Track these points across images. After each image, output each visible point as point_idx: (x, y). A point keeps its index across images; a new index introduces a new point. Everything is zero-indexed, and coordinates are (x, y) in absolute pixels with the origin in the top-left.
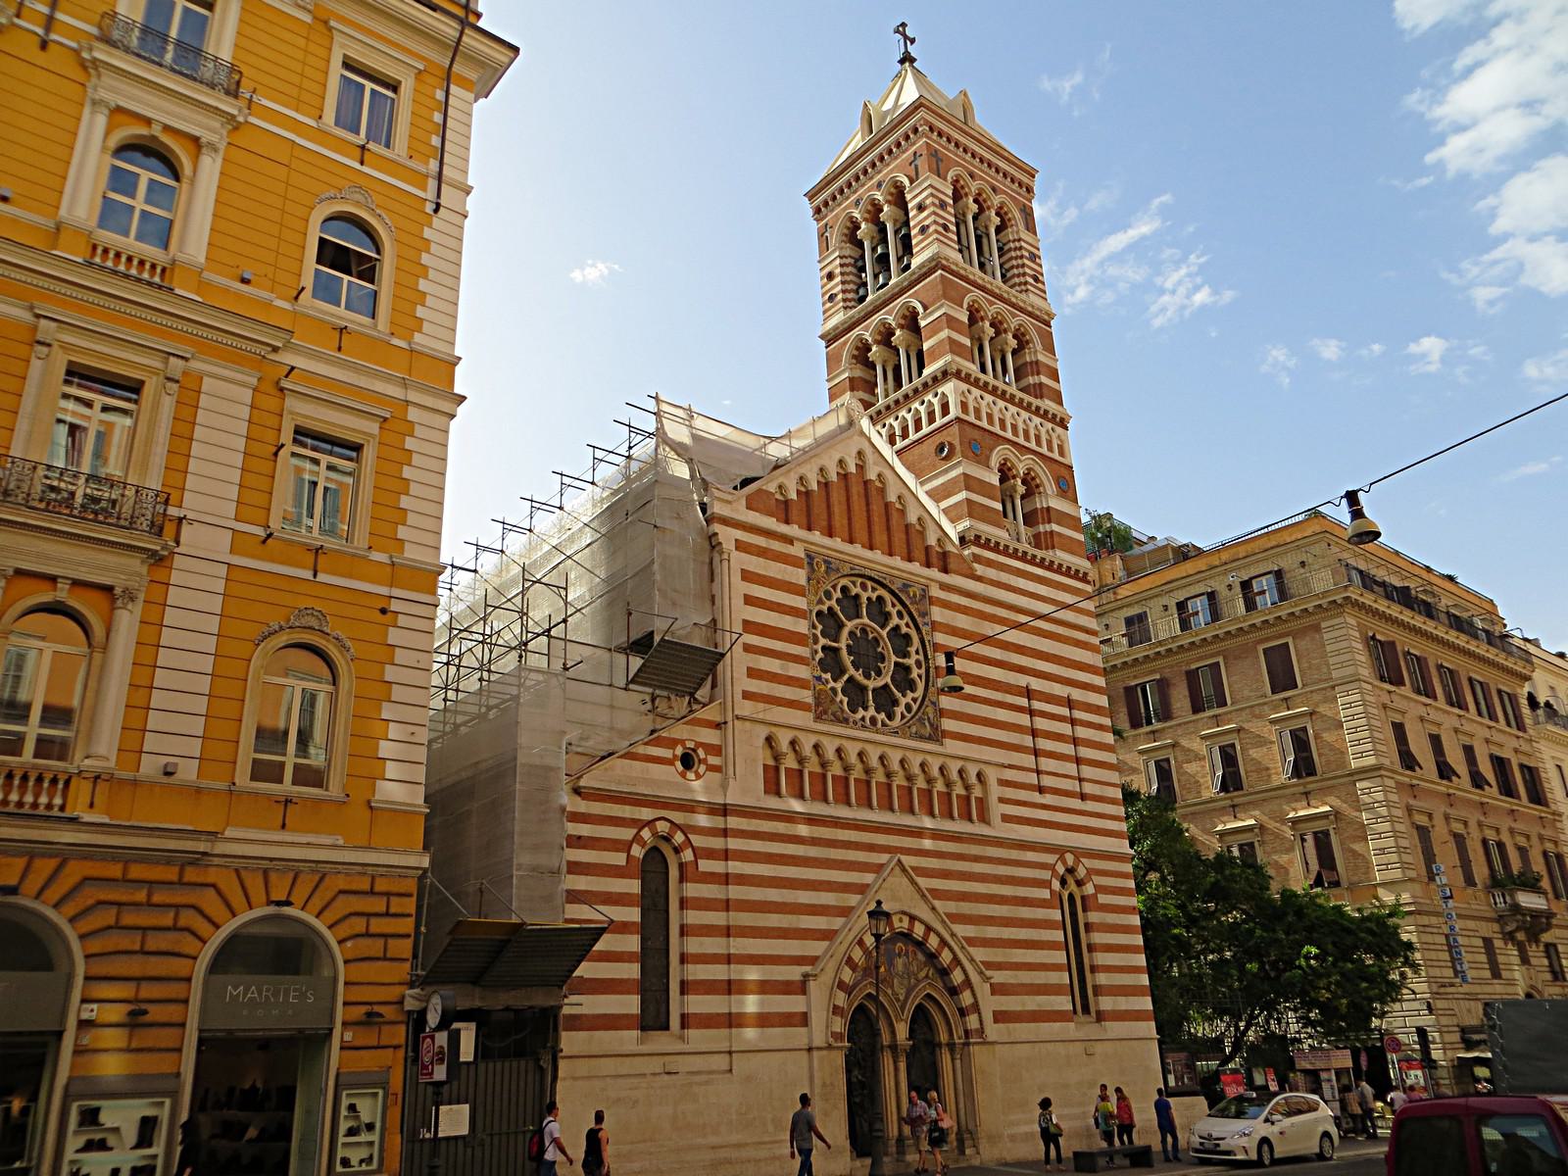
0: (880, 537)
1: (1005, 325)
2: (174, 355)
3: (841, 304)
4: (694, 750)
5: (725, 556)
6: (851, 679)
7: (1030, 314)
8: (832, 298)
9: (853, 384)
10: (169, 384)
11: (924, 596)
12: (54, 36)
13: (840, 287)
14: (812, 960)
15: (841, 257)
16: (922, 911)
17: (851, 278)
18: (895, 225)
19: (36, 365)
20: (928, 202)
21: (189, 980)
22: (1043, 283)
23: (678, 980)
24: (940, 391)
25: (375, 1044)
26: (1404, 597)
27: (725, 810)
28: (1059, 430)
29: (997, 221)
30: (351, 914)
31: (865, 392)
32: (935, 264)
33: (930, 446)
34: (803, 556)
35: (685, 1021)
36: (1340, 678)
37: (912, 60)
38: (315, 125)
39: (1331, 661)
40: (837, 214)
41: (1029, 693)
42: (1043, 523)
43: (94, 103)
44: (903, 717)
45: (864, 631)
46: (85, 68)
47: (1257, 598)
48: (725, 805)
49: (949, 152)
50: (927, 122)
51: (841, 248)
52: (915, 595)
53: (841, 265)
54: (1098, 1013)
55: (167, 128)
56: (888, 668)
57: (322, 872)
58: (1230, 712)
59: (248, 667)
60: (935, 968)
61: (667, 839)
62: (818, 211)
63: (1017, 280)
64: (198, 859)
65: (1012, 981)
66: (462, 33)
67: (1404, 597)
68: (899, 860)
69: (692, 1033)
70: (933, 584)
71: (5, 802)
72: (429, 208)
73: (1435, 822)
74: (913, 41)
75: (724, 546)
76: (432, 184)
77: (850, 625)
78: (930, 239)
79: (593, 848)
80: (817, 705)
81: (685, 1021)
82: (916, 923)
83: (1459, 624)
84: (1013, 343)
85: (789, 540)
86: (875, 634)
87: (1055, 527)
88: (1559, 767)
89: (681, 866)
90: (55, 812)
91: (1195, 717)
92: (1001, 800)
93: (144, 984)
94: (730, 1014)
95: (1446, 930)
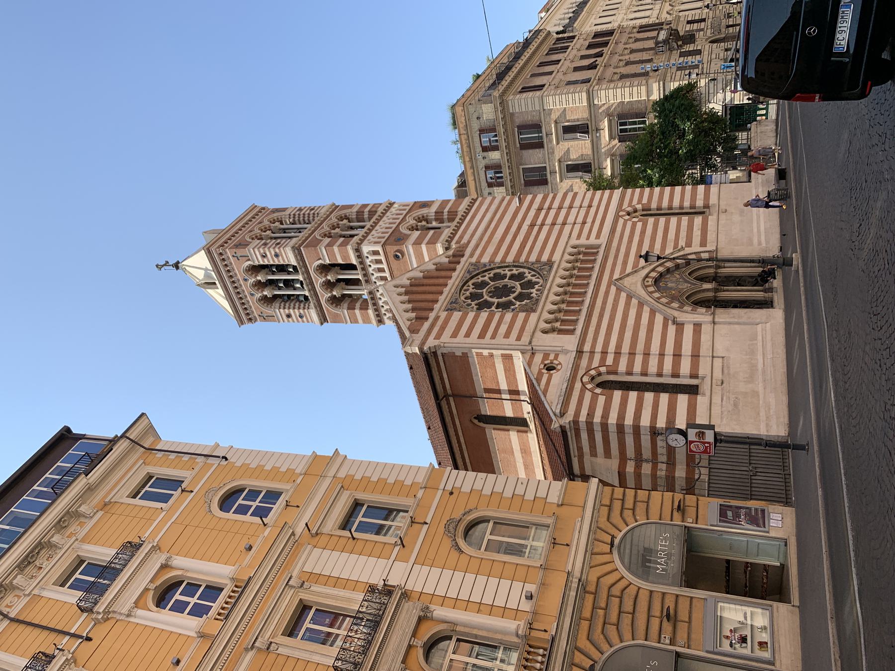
0: (441, 281)
1: (335, 224)
2: (288, 582)
4: (545, 365)
5: (442, 345)
6: (514, 298)
8: (301, 317)
9: (351, 308)
10: (305, 586)
12: (85, 635)
13: (296, 311)
14: (666, 320)
15: (280, 308)
16: (644, 273)
19: (281, 650)
20: (262, 251)
21: (651, 592)
23: (671, 379)
25: (695, 509)
26: (501, 76)
27: (580, 352)
28: (395, 206)
29: (277, 224)
30: (621, 516)
32: (297, 251)
33: (394, 263)
34: (447, 312)
35: (694, 376)
36: (540, 105)
38: (164, 513)
39: (530, 109)
40: (255, 307)
41: (532, 225)
42: (443, 216)
43: (129, 615)
44: (538, 278)
46: (108, 619)
48: (577, 351)
50: (218, 247)
51: (275, 308)
53: (284, 308)
54: (704, 207)
55: (151, 581)
56: (511, 283)
57: (595, 528)
58: (549, 165)
59: (474, 557)
60: (674, 271)
61: (593, 378)
62: (250, 319)
64: (582, 585)
65: (685, 240)
67: (501, 76)
68: (616, 280)
69: (701, 373)
70: (469, 261)
71: (541, 669)
72: (224, 462)
73: (619, 72)
74: (167, 262)
76: (211, 460)
77: (486, 297)
79: (595, 409)
81: (694, 376)
82: (650, 275)
83: (517, 56)
84: (345, 221)
85: (437, 318)
87: (446, 210)
88: (595, 25)
89: (608, 373)
90: (547, 653)
91: (550, 184)
92: (588, 238)
93: (653, 614)
94: (692, 356)
95: (674, 69)
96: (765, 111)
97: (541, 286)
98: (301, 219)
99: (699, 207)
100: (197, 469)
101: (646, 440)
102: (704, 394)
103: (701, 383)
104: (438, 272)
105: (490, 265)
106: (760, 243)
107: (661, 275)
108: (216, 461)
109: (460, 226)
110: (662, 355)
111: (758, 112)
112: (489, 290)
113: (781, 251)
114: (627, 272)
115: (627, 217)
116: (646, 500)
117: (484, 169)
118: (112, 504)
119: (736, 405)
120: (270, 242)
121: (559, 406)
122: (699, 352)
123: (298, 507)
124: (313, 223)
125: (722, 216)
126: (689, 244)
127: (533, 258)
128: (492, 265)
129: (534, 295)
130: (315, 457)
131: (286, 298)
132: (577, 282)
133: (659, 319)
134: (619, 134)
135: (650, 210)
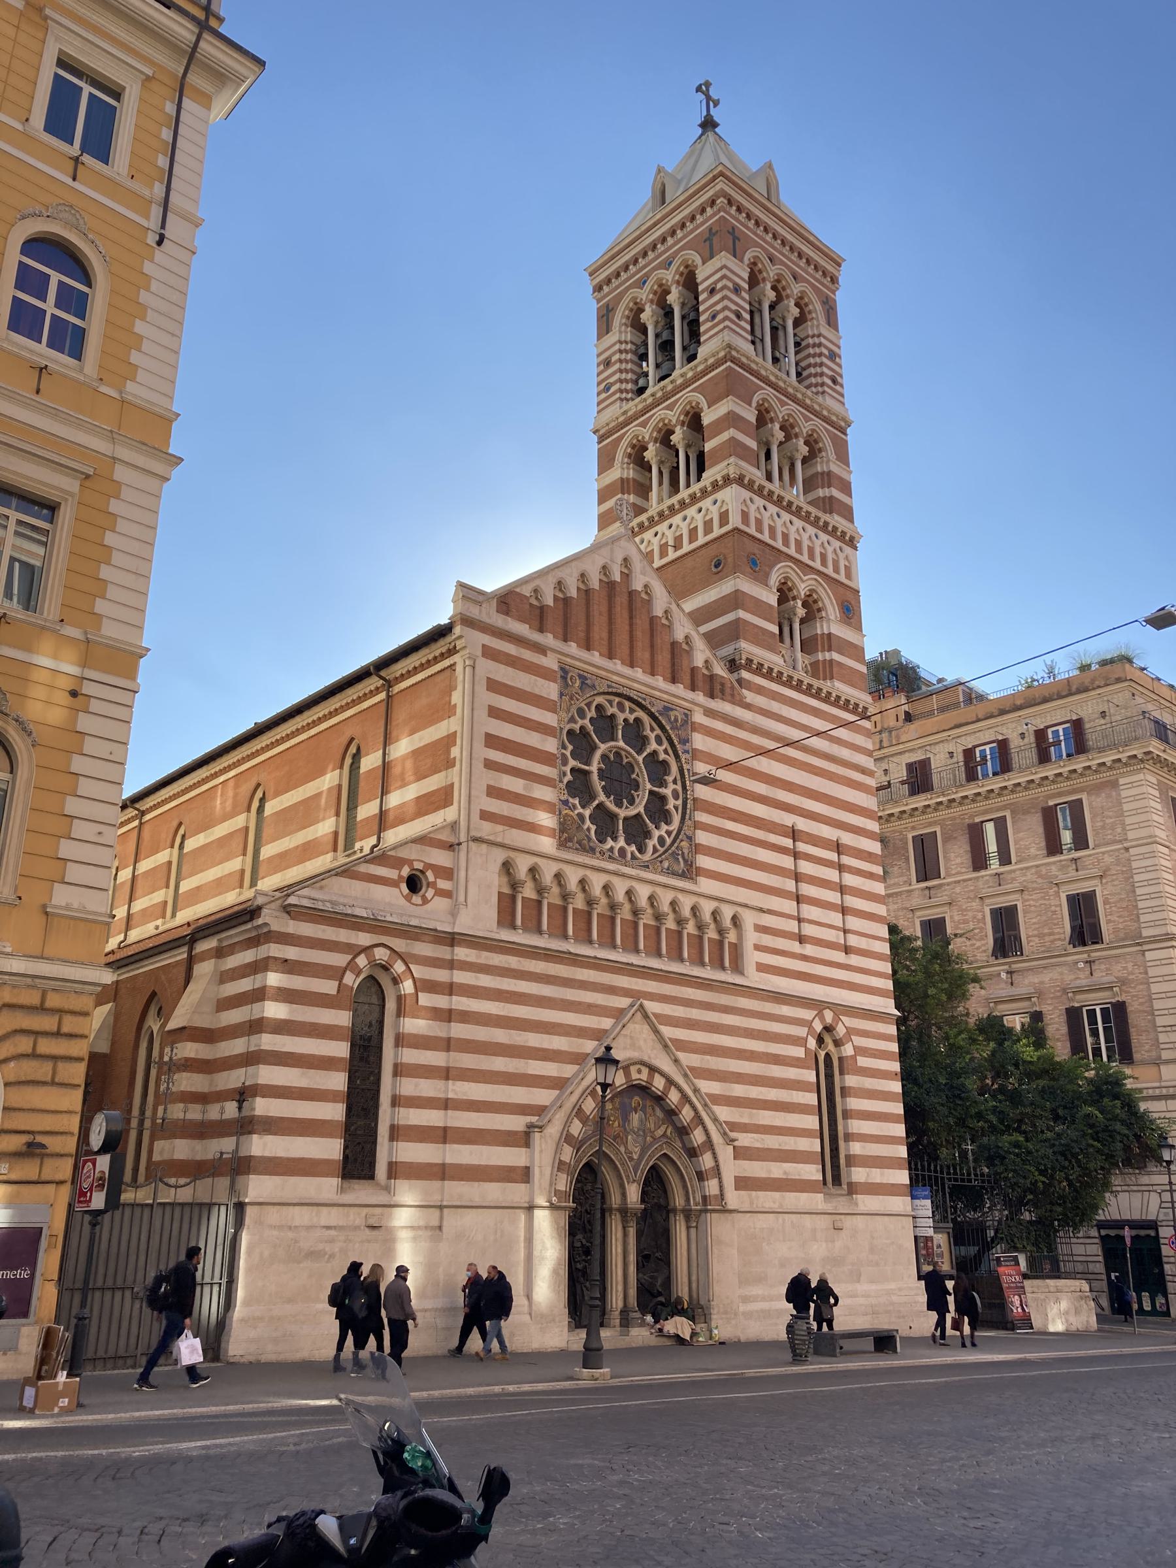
7: (826, 420)
11: (686, 722)
14: (540, 1110)
16: (665, 1065)
22: (842, 386)
25: (35, 1178)
27: (453, 939)
29: (796, 312)
35: (394, 1170)
38: (19, 127)
44: (655, 850)
45: (617, 754)
48: (454, 933)
52: (676, 720)
54: (850, 1184)
58: (1014, 871)
61: (385, 968)
68: (641, 1006)
70: (696, 708)
72: (152, 239)
74: (716, 104)
76: (156, 211)
77: (603, 747)
80: (562, 831)
81: (394, 1170)
85: (542, 650)
87: (836, 656)
89: (400, 999)
92: (757, 947)
94: (444, 1165)
96: (1149, 1309)
97: (633, 857)
98: (812, 360)
99: (849, 1174)
100: (134, 185)
101: (234, 1079)
102: (342, 1190)
103: (378, 1184)
104: (669, 647)
106: (746, 1299)
107: (659, 1099)
108: (154, 222)
109: (791, 687)
110: (446, 1104)
111: (1145, 1295)
112: (623, 753)
113: (720, 1343)
114: (663, 1029)
115: (818, 1027)
116: (57, 1080)
117: (1000, 738)
118: (43, 23)
119: (313, 1255)
120: (743, 299)
121: (306, 903)
122: (452, 1178)
123: (38, 392)
124: (801, 387)
125: (823, 1222)
126: (741, 1153)
127: (702, 837)
128: (688, 756)
129: (610, 843)
130: (165, 421)
131: (642, 351)
132: (618, 922)
133: (543, 1096)
134: (1084, 1009)
135: (842, 1073)
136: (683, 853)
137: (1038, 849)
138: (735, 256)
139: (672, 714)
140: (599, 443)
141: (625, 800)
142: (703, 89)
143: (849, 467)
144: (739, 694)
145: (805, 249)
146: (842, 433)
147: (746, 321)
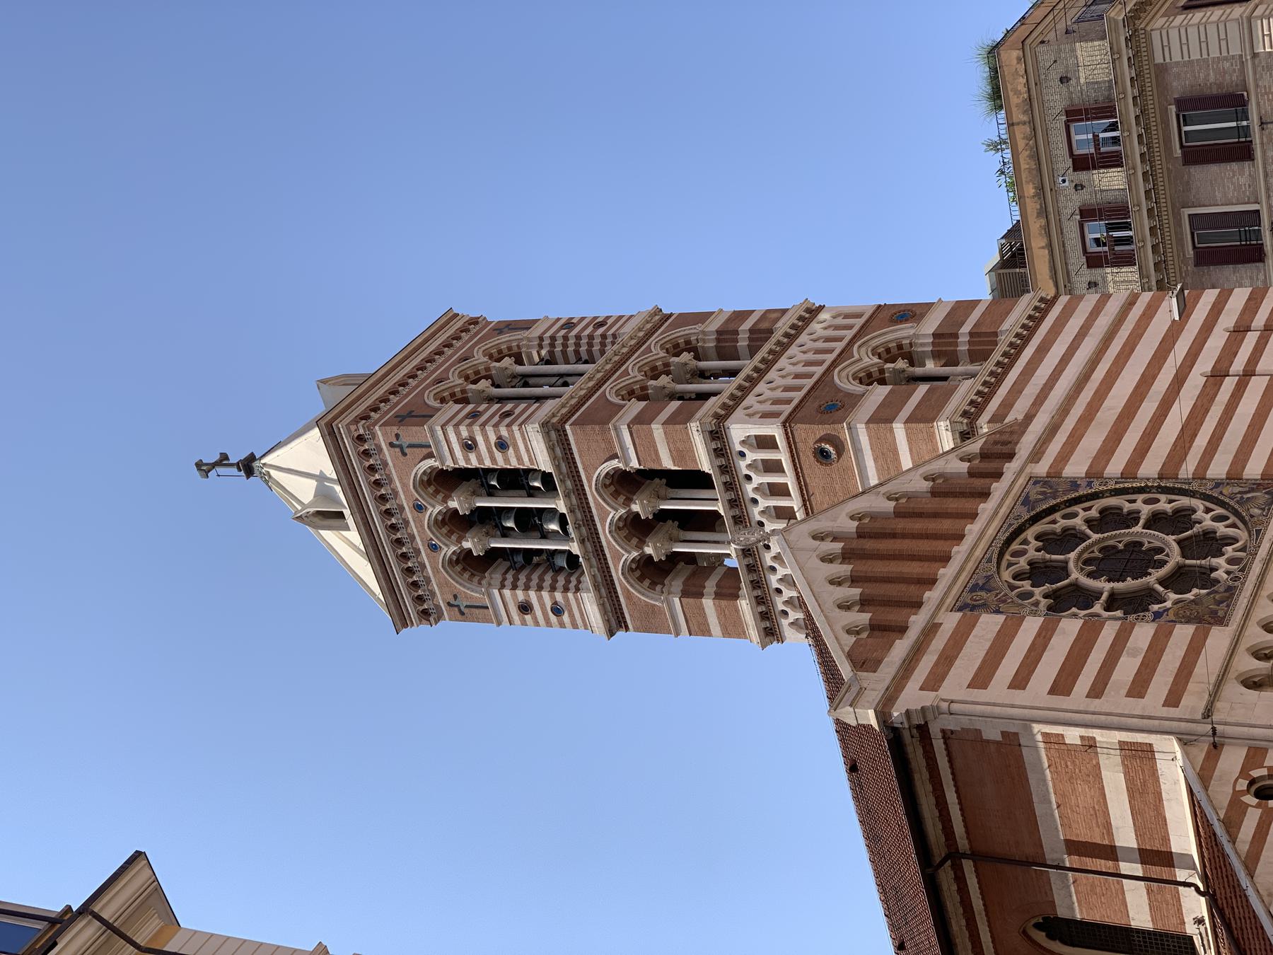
3: (570, 595)
4: (1253, 782)
5: (944, 705)
6: (1162, 582)
7: (650, 334)
8: (557, 611)
11: (1045, 483)
13: (545, 594)
15: (503, 586)
17: (535, 577)
18: (480, 495)
20: (465, 434)
22: (608, 318)
24: (738, 448)
29: (507, 362)
31: (707, 578)
32: (555, 434)
34: (959, 615)
37: (252, 458)
39: (1215, 53)
44: (1234, 526)
45: (1087, 562)
47: (1103, 150)
49: (400, 403)
56: (1153, 538)
62: (425, 615)
63: (596, 348)
66: (98, 917)
70: (1028, 470)
74: (225, 457)
75: (928, 704)
77: (1075, 575)
78: (517, 435)
84: (686, 357)
85: (931, 629)
86: (1095, 549)
87: (966, 329)
97: (1243, 549)
98: (571, 349)
105: (1089, 484)
112: (1086, 556)
124: (601, 361)
136: (1239, 493)
137: (1242, 174)
138: (432, 416)
139: (1033, 497)
140: (627, 629)
141: (1156, 557)
142: (204, 468)
143: (712, 313)
144: (1011, 426)
145: (432, 347)
146: (668, 318)
147: (515, 407)
